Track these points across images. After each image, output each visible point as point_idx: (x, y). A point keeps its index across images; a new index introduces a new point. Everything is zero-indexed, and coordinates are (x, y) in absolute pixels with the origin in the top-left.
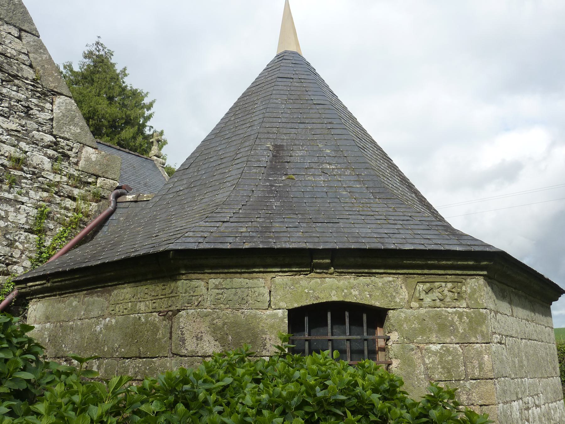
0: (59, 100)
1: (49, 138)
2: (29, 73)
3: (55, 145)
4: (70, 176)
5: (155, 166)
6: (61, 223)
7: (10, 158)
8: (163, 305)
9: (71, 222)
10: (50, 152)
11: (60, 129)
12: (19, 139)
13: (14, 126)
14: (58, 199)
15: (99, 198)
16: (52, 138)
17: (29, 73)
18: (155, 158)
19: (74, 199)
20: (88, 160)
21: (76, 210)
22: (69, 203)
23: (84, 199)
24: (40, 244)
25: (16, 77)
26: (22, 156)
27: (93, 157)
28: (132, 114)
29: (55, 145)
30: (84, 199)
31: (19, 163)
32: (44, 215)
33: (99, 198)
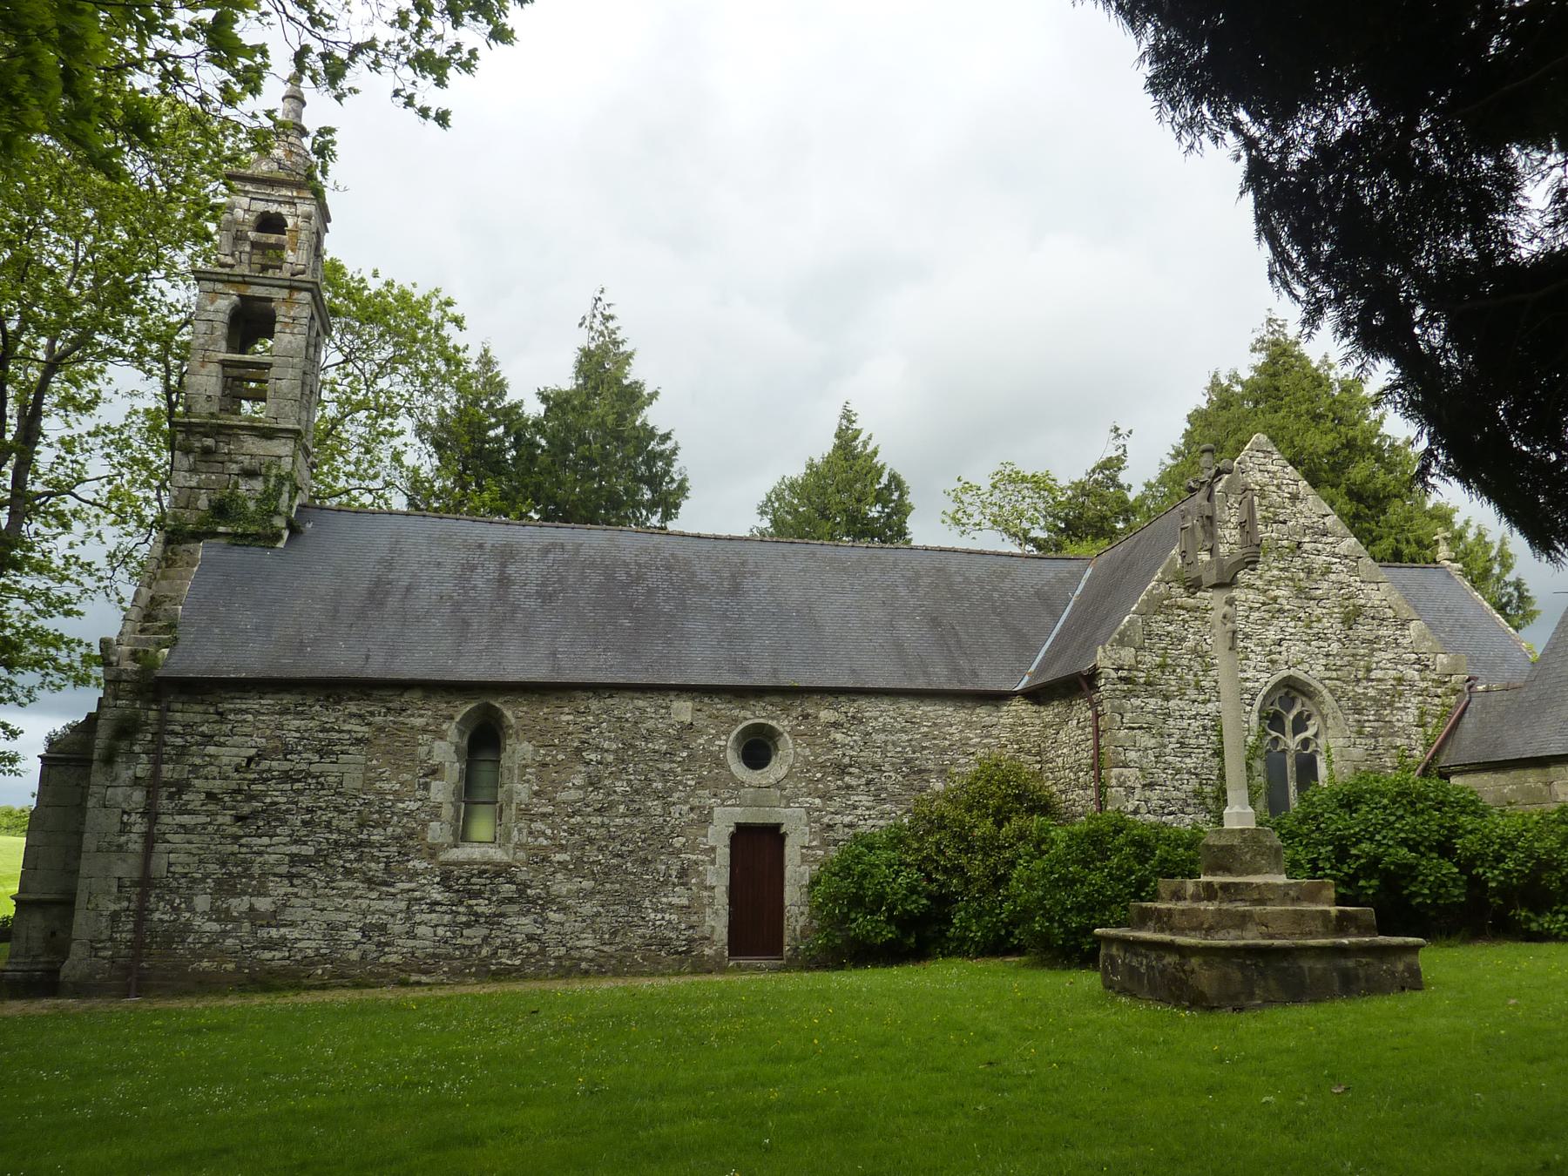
0: (1412, 625)
1: (1414, 656)
2: (1390, 613)
3: (1418, 662)
4: (1433, 680)
5: (1449, 575)
6: (1434, 716)
7: (1394, 679)
8: (1544, 779)
9: (1442, 715)
10: (1417, 667)
11: (1418, 647)
12: (1396, 664)
13: (1391, 656)
14: (1429, 700)
15: (1455, 692)
16: (1414, 656)
17: (1390, 613)
18: (1448, 563)
19: (1439, 697)
20: (1442, 664)
21: (1443, 705)
22: (1437, 700)
23: (1446, 695)
24: (1425, 734)
25: (1383, 620)
26: (1400, 675)
27: (1445, 661)
28: (1356, 432)
29: (1418, 662)
30: (1446, 695)
31: (1400, 680)
32: (1422, 714)
33: (1455, 692)
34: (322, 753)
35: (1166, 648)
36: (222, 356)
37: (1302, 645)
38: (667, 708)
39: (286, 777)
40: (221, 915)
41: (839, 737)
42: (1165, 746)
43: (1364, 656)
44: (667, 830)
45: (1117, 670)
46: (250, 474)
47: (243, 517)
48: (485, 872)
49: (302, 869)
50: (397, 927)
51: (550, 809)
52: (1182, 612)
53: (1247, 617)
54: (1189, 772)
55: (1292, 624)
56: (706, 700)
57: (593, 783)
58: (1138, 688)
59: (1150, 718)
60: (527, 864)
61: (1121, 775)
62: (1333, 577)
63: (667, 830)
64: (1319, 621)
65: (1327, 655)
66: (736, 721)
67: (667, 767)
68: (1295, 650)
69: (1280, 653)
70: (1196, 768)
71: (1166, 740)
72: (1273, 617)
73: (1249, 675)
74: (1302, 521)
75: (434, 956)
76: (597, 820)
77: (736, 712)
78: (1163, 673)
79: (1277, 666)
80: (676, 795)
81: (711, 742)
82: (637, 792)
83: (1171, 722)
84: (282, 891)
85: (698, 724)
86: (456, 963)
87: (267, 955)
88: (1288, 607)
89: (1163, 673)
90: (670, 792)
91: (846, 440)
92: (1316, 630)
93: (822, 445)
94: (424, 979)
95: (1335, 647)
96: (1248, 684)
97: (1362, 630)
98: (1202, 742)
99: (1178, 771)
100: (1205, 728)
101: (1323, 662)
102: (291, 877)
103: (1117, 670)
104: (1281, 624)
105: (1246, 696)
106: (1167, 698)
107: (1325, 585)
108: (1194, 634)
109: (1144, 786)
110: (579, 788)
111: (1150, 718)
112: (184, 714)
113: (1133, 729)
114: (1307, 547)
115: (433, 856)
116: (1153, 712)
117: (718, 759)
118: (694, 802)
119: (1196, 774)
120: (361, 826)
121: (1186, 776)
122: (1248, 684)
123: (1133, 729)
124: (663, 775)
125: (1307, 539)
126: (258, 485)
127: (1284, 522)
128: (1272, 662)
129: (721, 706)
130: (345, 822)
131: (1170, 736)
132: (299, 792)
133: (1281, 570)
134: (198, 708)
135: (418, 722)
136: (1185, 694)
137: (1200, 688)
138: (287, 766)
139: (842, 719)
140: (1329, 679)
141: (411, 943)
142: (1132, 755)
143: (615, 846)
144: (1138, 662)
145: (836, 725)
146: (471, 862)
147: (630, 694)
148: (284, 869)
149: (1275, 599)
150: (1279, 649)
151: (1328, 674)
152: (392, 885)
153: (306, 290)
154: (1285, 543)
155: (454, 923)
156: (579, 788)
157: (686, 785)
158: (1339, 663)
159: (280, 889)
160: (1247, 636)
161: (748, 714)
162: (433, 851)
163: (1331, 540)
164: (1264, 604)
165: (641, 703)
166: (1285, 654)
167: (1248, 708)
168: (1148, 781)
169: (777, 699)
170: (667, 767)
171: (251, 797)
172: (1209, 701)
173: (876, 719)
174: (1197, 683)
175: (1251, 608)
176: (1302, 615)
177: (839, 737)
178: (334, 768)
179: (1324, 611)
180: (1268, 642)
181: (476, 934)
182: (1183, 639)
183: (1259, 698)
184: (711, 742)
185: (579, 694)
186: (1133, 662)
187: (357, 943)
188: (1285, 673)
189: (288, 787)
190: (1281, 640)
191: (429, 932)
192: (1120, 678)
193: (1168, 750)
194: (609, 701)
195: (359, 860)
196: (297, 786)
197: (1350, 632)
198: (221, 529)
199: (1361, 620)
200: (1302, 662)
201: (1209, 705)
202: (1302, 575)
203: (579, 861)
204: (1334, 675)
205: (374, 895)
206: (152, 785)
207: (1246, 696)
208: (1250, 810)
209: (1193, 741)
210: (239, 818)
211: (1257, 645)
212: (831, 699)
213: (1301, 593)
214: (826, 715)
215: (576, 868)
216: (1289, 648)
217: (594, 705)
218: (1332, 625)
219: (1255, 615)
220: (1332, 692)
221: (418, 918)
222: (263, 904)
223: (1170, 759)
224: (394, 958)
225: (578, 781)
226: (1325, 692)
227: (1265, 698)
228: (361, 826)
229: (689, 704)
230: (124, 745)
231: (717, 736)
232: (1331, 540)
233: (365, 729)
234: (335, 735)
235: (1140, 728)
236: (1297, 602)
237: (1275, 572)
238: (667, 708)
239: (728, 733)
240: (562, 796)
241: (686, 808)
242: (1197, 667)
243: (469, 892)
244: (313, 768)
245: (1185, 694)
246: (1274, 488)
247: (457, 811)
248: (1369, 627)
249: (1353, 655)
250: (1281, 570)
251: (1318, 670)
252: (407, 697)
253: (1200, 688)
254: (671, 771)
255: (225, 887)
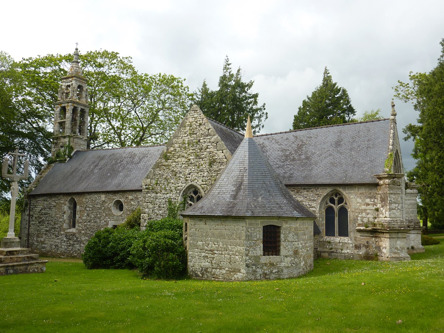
34: (50, 209)
35: (158, 178)
36: (58, 121)
37: (196, 174)
38: (100, 197)
39: (45, 214)
40: (37, 241)
41: (133, 203)
42: (155, 207)
43: (215, 176)
44: (100, 226)
45: (146, 186)
46: (62, 147)
47: (61, 157)
48: (71, 235)
49: (47, 233)
50: (59, 246)
51: (81, 221)
52: (164, 167)
53: (181, 166)
54: (160, 215)
55: (194, 167)
56: (108, 194)
57: (88, 215)
58: (150, 191)
59: (152, 199)
60: (78, 233)
61: (143, 216)
62: (208, 150)
63: (100, 226)
64: (202, 165)
65: (203, 177)
66: (114, 199)
67: (100, 211)
68: (194, 175)
69: (189, 177)
70: (162, 214)
71: (155, 206)
72: (189, 166)
73: (179, 185)
74: (201, 132)
75: (64, 252)
76: (89, 224)
77: (114, 197)
78: (157, 185)
79: (188, 181)
80: (102, 218)
81: (108, 205)
82: (95, 217)
83: (157, 200)
84: (45, 237)
85: (106, 200)
86: (67, 254)
87: (43, 250)
88: (193, 162)
89: (157, 185)
90: (101, 217)
91: (327, 80)
92: (200, 169)
93: (319, 82)
94: (63, 257)
95: (206, 174)
96: (179, 188)
97: (215, 167)
98: (164, 206)
99: (157, 215)
100: (166, 201)
101: (202, 179)
102: (46, 234)
103: (146, 186)
104: (191, 168)
105: (178, 191)
106: (157, 193)
107: (205, 153)
108: (166, 173)
109: (148, 219)
110: (86, 216)
111: (152, 199)
112: (33, 201)
113: (148, 202)
114: (201, 141)
115: (64, 231)
116: (153, 198)
117: (110, 209)
118: (105, 220)
119: (162, 216)
120: (55, 224)
121: (159, 216)
122: (179, 188)
123: (148, 202)
124: (100, 213)
125: (202, 138)
126: (63, 149)
127: (196, 134)
128: (187, 180)
129: (111, 196)
130: (53, 224)
131: (157, 204)
132: (47, 217)
133: (193, 150)
134: (34, 200)
135: (62, 202)
136: (162, 192)
137: (165, 190)
138: (45, 212)
139: (133, 198)
140: (203, 184)
141: (61, 249)
142: (147, 210)
143: (92, 230)
144: (151, 183)
145: (132, 200)
146: (70, 232)
147: (94, 194)
148: (44, 233)
149: (189, 160)
150: (189, 176)
151: (203, 183)
152: (58, 237)
153: (70, 102)
154: (194, 141)
155: (67, 246)
156: (86, 216)
157: (103, 216)
158: (206, 179)
159: (44, 237)
160: (180, 173)
161: (116, 197)
162: (64, 230)
163: (209, 137)
164: (186, 162)
165: (96, 196)
166: (191, 177)
167: (178, 195)
168: (149, 217)
169: (121, 193)
170: (100, 211)
171: (40, 218)
172: (168, 193)
173: (141, 198)
174: (165, 188)
175: (183, 163)
176: (198, 164)
177: (133, 203)
178: (51, 212)
179: (204, 162)
180: (186, 174)
181: (71, 248)
182: (163, 175)
183: (182, 192)
184: (108, 205)
185: (86, 194)
186: (149, 183)
187: (54, 248)
188: (190, 183)
189: (45, 216)
190: (190, 173)
191: (64, 247)
192: (146, 188)
193: (155, 209)
194: (91, 196)
195: (54, 231)
196: (47, 216)
197: (211, 168)
198: (58, 160)
199: (215, 164)
200: (195, 179)
201: (168, 195)
202: (199, 151)
203: (86, 233)
204: (204, 183)
205: (56, 239)
206: (29, 215)
207: (178, 191)
208: (14, 233)
209: (162, 206)
210: (39, 222)
211: (183, 175)
212: (131, 193)
213: (198, 157)
214: (130, 197)
215: (85, 234)
216: (192, 175)
217: (88, 197)
218: (205, 167)
219: (184, 165)
220: (203, 188)
221: (63, 244)
222: (42, 239)
223: (156, 211)
224: (59, 252)
225: (86, 215)
226: (201, 189)
227: (184, 192)
228: (55, 224)
229: (104, 196)
230: (26, 208)
231: (110, 203)
232: (209, 137)
233: (55, 204)
234: (51, 205)
235: (149, 202)
236: (196, 160)
237: (191, 151)
238: (100, 197)
239: (112, 203)
240: (83, 218)
241: (104, 221)
242: (166, 183)
243: (69, 239)
244: (49, 212)
245: (162, 192)
246: (194, 123)
247: (70, 221)
248: (218, 166)
249: (211, 176)
250: (193, 150)
251: (200, 182)
252: (61, 196)
253: (165, 190)
254: (101, 212)
255: (38, 237)
